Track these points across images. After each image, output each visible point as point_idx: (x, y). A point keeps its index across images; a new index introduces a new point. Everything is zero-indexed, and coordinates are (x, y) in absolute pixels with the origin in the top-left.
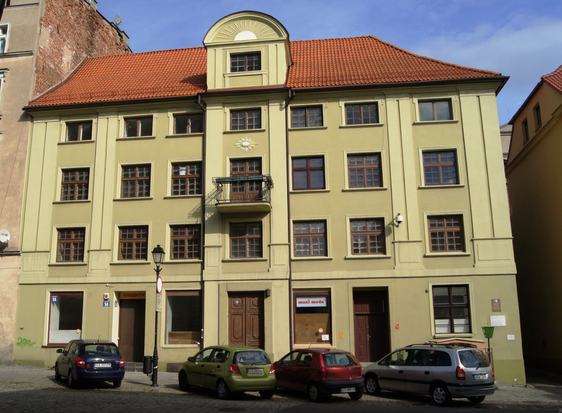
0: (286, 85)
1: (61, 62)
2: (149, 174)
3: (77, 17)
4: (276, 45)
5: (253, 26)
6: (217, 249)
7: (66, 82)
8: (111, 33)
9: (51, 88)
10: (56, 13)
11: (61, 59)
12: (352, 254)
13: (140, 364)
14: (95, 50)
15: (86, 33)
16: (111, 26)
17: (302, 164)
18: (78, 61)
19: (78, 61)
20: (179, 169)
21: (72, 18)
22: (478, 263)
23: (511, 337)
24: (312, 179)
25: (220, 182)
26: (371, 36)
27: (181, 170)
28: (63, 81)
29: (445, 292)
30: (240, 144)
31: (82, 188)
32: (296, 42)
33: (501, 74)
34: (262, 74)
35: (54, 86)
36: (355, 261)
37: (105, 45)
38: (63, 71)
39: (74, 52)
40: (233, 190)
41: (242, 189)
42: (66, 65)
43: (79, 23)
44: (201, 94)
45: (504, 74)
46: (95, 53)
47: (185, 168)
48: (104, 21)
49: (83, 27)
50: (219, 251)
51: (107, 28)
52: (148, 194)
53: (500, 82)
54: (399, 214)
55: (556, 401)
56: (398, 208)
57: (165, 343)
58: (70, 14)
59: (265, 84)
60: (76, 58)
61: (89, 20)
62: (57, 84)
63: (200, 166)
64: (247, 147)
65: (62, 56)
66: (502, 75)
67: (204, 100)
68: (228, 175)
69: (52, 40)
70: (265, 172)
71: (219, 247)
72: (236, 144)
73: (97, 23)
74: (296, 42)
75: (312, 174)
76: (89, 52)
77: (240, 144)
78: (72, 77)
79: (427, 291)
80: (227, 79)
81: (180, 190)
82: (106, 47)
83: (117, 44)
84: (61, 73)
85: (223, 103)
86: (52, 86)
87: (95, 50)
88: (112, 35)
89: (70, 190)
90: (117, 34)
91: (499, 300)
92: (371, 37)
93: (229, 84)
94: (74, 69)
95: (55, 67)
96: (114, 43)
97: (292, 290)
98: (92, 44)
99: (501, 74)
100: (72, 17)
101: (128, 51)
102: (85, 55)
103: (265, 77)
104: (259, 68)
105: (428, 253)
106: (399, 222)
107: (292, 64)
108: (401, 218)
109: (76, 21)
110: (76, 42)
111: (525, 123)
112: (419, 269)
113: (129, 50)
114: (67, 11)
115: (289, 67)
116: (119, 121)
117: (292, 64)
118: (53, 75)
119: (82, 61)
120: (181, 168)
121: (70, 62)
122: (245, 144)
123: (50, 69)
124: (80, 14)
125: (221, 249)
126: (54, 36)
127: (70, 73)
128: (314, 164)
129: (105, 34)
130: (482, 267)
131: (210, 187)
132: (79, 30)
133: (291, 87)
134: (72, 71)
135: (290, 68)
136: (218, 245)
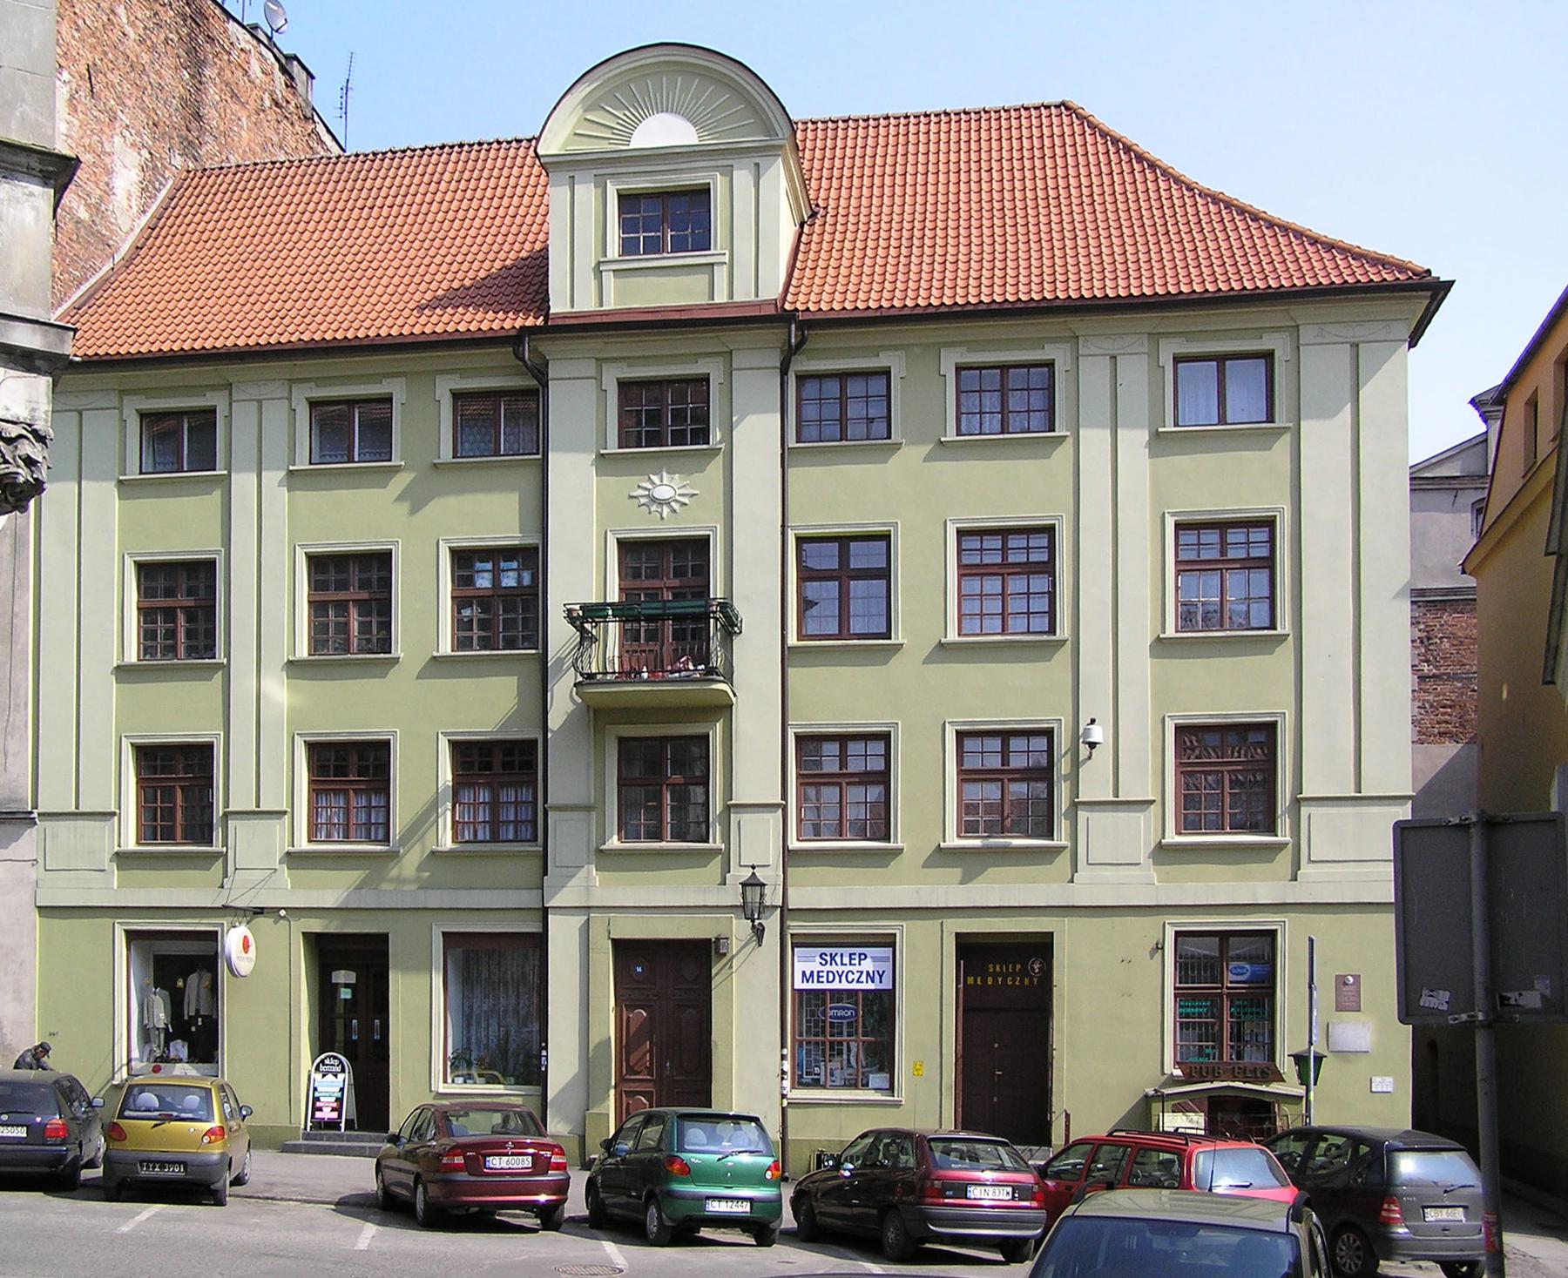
0: (784, 300)
1: (109, 191)
2: (386, 583)
3: (145, 28)
4: (757, 165)
5: (686, 97)
6: (582, 815)
7: (129, 261)
8: (255, 68)
9: (83, 288)
10: (80, 22)
11: (107, 184)
12: (959, 836)
13: (378, 1137)
14: (208, 138)
15: (175, 81)
16: (255, 42)
17: (827, 558)
18: (161, 184)
19: (161, 184)
20: (471, 566)
21: (132, 34)
22: (1306, 870)
23: (1382, 1083)
24: (855, 607)
25: (586, 617)
26: (1076, 102)
27: (478, 572)
28: (118, 258)
29: (1209, 948)
30: (647, 493)
31: (196, 621)
32: (833, 122)
33: (1429, 272)
34: (712, 264)
35: (93, 281)
36: (1160, 771)
37: (239, 114)
38: (117, 225)
39: (145, 153)
40: (629, 636)
41: (652, 636)
42: (125, 203)
43: (153, 49)
44: (533, 330)
45: (1441, 273)
46: (209, 147)
47: (489, 566)
48: (232, 26)
49: (166, 61)
50: (589, 821)
51: (242, 50)
52: (385, 645)
53: (1425, 297)
54: (1093, 721)
55: (554, 1197)
56: (1095, 702)
57: (445, 1081)
58: (125, 21)
59: (721, 297)
60: (152, 172)
61: (185, 30)
62: (101, 273)
63: (532, 556)
64: (667, 502)
65: (109, 172)
66: (1433, 275)
67: (540, 349)
68: (614, 596)
69: (76, 122)
70: (717, 591)
71: (588, 808)
72: (635, 494)
73: (211, 39)
74: (833, 122)
75: (857, 587)
76: (190, 147)
77: (647, 493)
78: (144, 244)
79: (1159, 948)
80: (609, 279)
81: (476, 633)
82: (244, 119)
83: (277, 104)
84: (111, 231)
85: (597, 359)
86: (87, 280)
87: (208, 138)
88: (260, 74)
89: (160, 626)
90: (277, 66)
91: (1357, 978)
92: (1067, 108)
93: (618, 297)
94: (149, 215)
95: (91, 216)
96: (268, 103)
97: (789, 936)
98: (198, 117)
99: (1429, 272)
100: (129, 30)
101: (314, 122)
102: (178, 161)
103: (721, 274)
104: (704, 244)
105: (1172, 838)
106: (1092, 745)
107: (814, 215)
108: (1097, 734)
109: (142, 42)
110: (149, 117)
111: (1533, 404)
112: (1149, 885)
113: (316, 119)
114: (113, 12)
115: (802, 225)
116: (295, 410)
117: (814, 215)
118: (89, 242)
119: (170, 182)
120: (479, 566)
121: (136, 191)
122: (663, 492)
123: (77, 222)
124: (156, 14)
125: (594, 814)
126: (80, 108)
127: (137, 231)
128: (861, 557)
129: (239, 73)
130: (1316, 884)
131: (560, 634)
132: (157, 73)
133: (796, 310)
134: (145, 219)
135: (806, 227)
136: (582, 801)
